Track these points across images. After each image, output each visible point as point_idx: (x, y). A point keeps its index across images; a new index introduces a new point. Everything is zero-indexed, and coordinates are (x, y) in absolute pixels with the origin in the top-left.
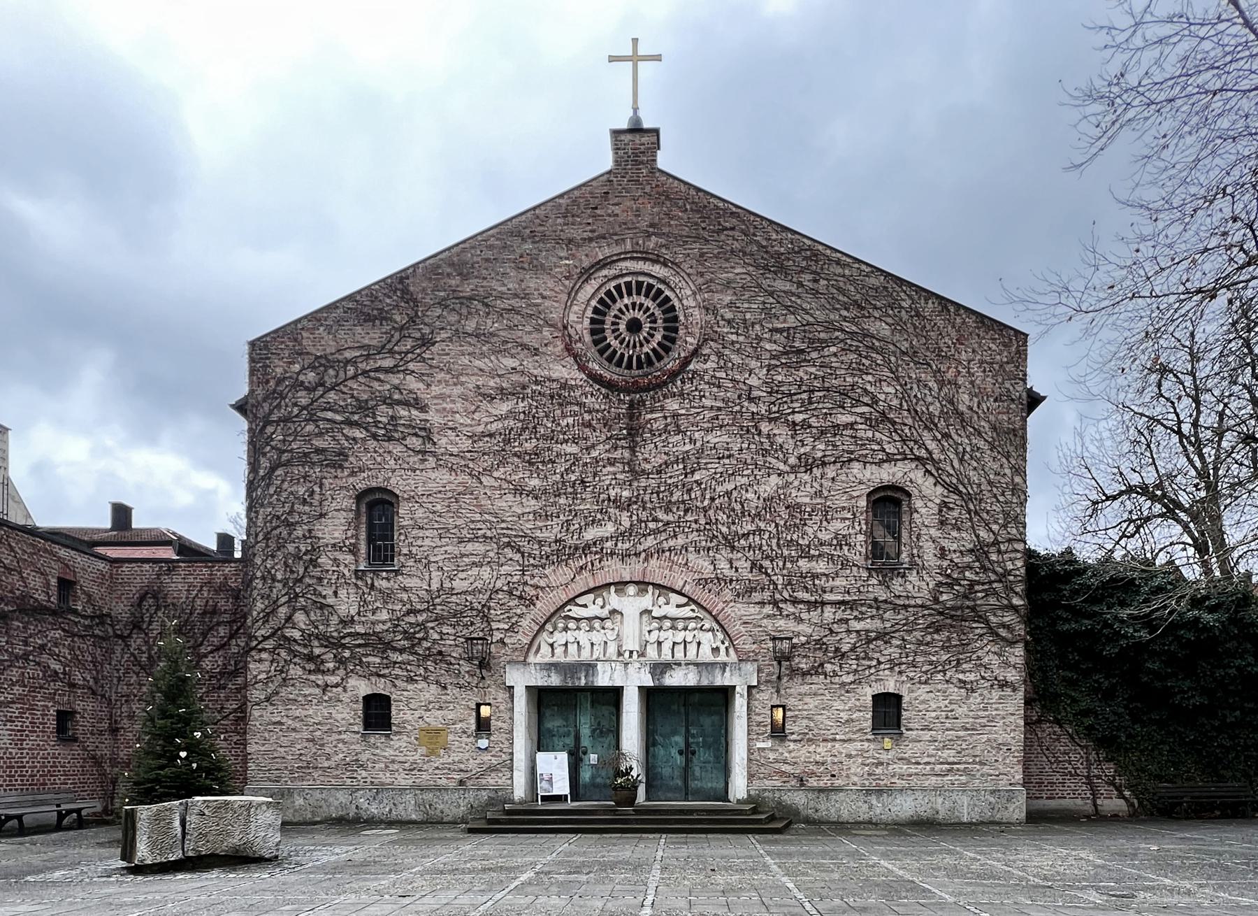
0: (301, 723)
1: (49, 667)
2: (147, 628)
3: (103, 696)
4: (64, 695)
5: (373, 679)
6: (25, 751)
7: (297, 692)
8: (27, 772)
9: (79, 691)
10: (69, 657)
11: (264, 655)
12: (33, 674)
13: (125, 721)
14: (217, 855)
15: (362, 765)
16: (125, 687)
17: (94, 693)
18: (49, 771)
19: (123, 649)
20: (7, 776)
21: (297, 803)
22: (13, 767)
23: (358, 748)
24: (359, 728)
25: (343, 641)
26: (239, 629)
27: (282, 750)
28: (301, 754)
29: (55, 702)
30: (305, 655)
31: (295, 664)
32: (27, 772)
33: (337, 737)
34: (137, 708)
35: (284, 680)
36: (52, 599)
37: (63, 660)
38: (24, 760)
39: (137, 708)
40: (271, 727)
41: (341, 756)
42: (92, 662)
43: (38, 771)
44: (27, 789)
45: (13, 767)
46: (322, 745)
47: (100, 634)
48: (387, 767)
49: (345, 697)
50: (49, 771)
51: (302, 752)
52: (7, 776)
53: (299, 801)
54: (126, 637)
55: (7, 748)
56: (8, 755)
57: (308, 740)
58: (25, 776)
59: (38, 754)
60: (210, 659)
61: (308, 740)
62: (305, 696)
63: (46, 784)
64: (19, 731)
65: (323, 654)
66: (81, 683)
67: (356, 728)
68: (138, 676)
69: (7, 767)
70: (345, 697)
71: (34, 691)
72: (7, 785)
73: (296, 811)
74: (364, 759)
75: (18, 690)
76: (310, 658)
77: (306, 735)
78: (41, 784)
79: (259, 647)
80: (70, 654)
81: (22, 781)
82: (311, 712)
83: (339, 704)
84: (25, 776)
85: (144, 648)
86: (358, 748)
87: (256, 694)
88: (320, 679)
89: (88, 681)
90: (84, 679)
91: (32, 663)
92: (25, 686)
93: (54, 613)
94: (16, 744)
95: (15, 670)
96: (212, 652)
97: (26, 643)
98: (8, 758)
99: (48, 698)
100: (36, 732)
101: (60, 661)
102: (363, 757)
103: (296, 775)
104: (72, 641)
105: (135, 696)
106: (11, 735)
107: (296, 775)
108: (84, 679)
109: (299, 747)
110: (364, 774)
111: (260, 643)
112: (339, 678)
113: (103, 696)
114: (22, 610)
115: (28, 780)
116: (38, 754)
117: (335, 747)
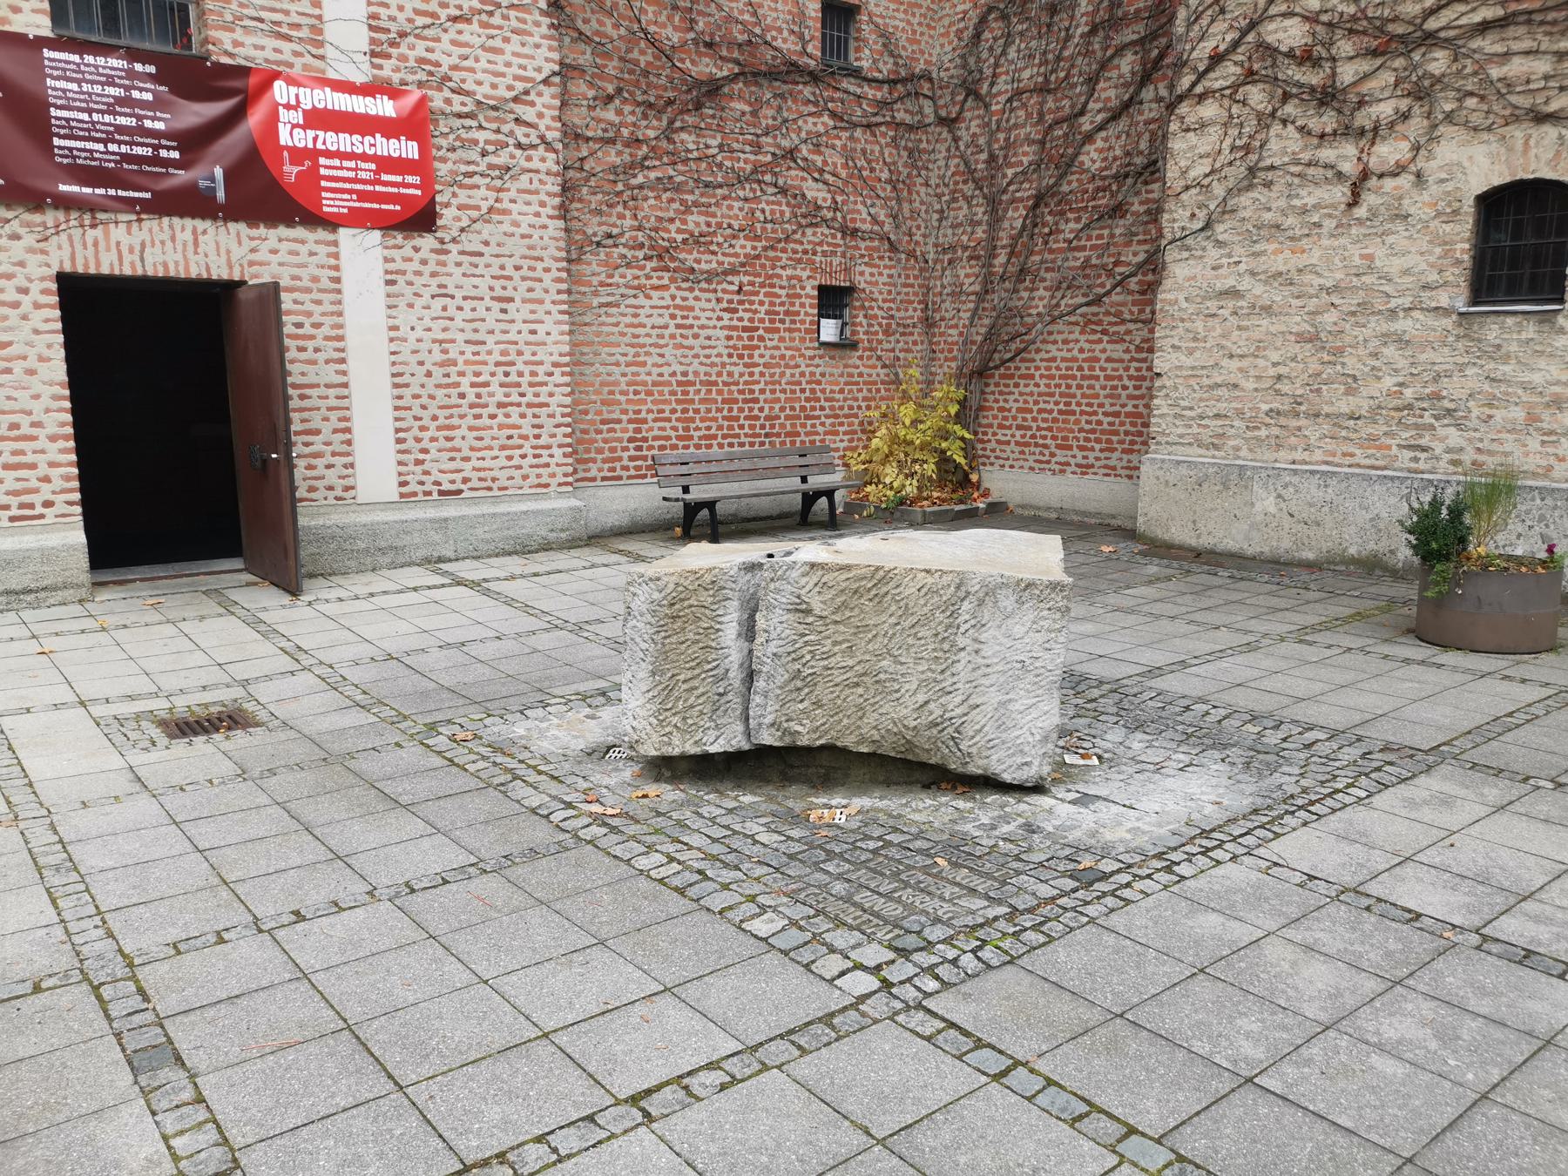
0: (1287, 291)
1: (804, 196)
2: (989, 92)
3: (911, 254)
4: (834, 253)
5: (1517, 133)
6: (757, 370)
7: (1282, 203)
8: (761, 410)
9: (862, 245)
10: (843, 174)
11: (1209, 110)
12: (773, 212)
13: (947, 304)
14: (844, 751)
15: (1449, 412)
16: (950, 232)
17: (893, 248)
18: (803, 408)
19: (948, 150)
20: (724, 418)
21: (1258, 507)
22: (736, 401)
23: (1443, 358)
24: (1456, 296)
25: (1432, 24)
26: (1161, 56)
27: (1235, 364)
28: (1279, 378)
29: (814, 270)
30: (1313, 89)
31: (1284, 122)
32: (761, 410)
33: (1385, 327)
34: (967, 276)
35: (1252, 171)
36: (810, 49)
37: (831, 179)
38: (756, 387)
39: (967, 276)
40: (1212, 305)
41: (1389, 382)
42: (889, 181)
43: (782, 409)
44: (762, 444)
45: (736, 401)
46: (1339, 351)
47: (908, 119)
48: (1532, 419)
49: (1419, 205)
50: (803, 408)
51: (1282, 370)
52: (724, 418)
53: (1266, 503)
54: (955, 120)
55: (724, 365)
56: (725, 378)
57: (1301, 338)
58: (757, 418)
59: (782, 374)
60: (1100, 144)
61: (1301, 338)
62: (1304, 211)
63: (798, 434)
64: (745, 329)
65: (1366, 77)
66: (867, 227)
67: (1443, 299)
68: (970, 206)
69: (724, 401)
70: (1419, 205)
71: (773, 248)
72: (724, 437)
73: (1254, 526)
74: (1463, 394)
75: (743, 247)
76: (1326, 97)
77: (1298, 323)
78: (788, 434)
79: (1199, 89)
80: (846, 166)
81: (752, 427)
82: (1314, 257)
83: (1399, 226)
84: (757, 418)
85: (982, 141)
86: (1443, 358)
87: (1177, 218)
88: (1345, 155)
89: (881, 224)
90: (875, 221)
91: (771, 190)
92: (757, 238)
93: (814, 78)
94: (741, 357)
95: (736, 204)
96: (1101, 128)
97: (758, 148)
98: (725, 384)
99: (799, 261)
100: (777, 330)
101: (825, 183)
102: (1455, 388)
103: (1263, 433)
104: (851, 138)
105: (965, 248)
106: (729, 338)
107: (1263, 433)
108: (875, 221)
109: (1275, 357)
110: (1454, 437)
111: (1201, 76)
112: (1405, 146)
113: (911, 254)
114: (751, 74)
115: (763, 427)
116: (782, 374)
117: (1375, 355)
